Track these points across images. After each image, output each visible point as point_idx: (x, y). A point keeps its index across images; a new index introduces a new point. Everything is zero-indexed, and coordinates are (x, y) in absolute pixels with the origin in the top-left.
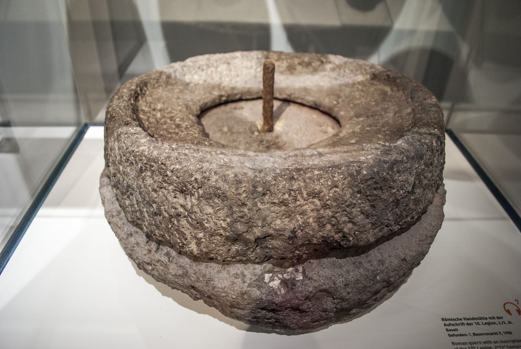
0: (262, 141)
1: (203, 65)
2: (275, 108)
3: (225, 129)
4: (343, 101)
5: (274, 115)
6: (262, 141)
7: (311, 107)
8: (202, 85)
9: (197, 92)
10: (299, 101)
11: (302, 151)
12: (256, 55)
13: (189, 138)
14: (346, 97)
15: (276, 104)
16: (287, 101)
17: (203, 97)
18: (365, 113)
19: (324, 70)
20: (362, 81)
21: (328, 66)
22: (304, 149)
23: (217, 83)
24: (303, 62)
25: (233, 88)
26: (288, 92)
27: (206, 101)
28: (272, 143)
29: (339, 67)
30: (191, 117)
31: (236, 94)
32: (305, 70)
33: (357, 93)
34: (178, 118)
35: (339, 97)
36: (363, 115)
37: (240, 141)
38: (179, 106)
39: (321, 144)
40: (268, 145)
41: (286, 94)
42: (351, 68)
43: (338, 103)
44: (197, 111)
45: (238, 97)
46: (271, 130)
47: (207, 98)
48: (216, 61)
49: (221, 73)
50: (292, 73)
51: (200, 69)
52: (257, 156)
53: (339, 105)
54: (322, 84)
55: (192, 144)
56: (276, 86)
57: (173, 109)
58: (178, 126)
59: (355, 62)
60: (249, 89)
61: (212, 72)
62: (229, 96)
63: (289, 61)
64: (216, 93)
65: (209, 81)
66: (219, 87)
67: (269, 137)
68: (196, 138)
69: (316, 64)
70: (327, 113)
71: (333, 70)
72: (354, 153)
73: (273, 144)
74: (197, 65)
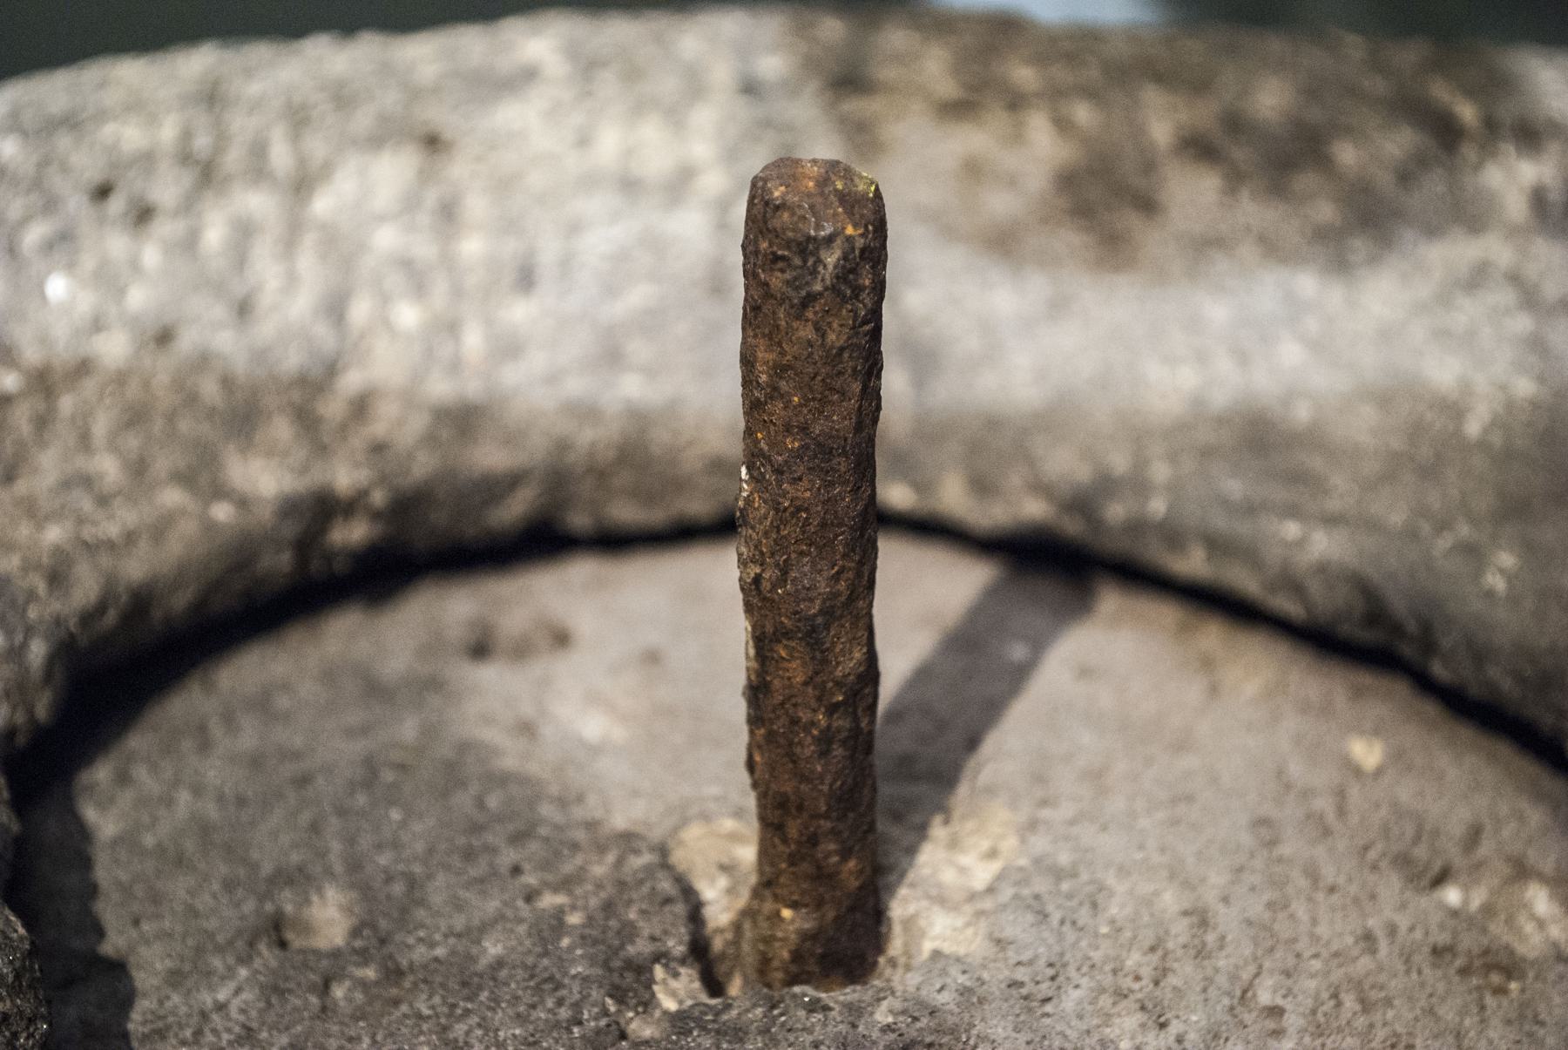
1: (146, 160)
3: (329, 918)
5: (889, 743)
8: (120, 379)
9: (49, 466)
10: (1193, 564)
15: (919, 603)
16: (1060, 563)
19: (1470, 215)
21: (1513, 178)
23: (292, 360)
24: (1235, 124)
25: (462, 420)
26: (1066, 464)
27: (135, 568)
31: (497, 487)
32: (1252, 211)
45: (514, 510)
46: (849, 942)
48: (298, 119)
49: (341, 249)
50: (1113, 250)
51: (116, 204)
54: (1443, 371)
56: (895, 382)
60: (639, 418)
61: (244, 232)
62: (407, 505)
63: (1083, 113)
64: (265, 478)
65: (210, 331)
66: (306, 399)
69: (1374, 150)
74: (87, 164)
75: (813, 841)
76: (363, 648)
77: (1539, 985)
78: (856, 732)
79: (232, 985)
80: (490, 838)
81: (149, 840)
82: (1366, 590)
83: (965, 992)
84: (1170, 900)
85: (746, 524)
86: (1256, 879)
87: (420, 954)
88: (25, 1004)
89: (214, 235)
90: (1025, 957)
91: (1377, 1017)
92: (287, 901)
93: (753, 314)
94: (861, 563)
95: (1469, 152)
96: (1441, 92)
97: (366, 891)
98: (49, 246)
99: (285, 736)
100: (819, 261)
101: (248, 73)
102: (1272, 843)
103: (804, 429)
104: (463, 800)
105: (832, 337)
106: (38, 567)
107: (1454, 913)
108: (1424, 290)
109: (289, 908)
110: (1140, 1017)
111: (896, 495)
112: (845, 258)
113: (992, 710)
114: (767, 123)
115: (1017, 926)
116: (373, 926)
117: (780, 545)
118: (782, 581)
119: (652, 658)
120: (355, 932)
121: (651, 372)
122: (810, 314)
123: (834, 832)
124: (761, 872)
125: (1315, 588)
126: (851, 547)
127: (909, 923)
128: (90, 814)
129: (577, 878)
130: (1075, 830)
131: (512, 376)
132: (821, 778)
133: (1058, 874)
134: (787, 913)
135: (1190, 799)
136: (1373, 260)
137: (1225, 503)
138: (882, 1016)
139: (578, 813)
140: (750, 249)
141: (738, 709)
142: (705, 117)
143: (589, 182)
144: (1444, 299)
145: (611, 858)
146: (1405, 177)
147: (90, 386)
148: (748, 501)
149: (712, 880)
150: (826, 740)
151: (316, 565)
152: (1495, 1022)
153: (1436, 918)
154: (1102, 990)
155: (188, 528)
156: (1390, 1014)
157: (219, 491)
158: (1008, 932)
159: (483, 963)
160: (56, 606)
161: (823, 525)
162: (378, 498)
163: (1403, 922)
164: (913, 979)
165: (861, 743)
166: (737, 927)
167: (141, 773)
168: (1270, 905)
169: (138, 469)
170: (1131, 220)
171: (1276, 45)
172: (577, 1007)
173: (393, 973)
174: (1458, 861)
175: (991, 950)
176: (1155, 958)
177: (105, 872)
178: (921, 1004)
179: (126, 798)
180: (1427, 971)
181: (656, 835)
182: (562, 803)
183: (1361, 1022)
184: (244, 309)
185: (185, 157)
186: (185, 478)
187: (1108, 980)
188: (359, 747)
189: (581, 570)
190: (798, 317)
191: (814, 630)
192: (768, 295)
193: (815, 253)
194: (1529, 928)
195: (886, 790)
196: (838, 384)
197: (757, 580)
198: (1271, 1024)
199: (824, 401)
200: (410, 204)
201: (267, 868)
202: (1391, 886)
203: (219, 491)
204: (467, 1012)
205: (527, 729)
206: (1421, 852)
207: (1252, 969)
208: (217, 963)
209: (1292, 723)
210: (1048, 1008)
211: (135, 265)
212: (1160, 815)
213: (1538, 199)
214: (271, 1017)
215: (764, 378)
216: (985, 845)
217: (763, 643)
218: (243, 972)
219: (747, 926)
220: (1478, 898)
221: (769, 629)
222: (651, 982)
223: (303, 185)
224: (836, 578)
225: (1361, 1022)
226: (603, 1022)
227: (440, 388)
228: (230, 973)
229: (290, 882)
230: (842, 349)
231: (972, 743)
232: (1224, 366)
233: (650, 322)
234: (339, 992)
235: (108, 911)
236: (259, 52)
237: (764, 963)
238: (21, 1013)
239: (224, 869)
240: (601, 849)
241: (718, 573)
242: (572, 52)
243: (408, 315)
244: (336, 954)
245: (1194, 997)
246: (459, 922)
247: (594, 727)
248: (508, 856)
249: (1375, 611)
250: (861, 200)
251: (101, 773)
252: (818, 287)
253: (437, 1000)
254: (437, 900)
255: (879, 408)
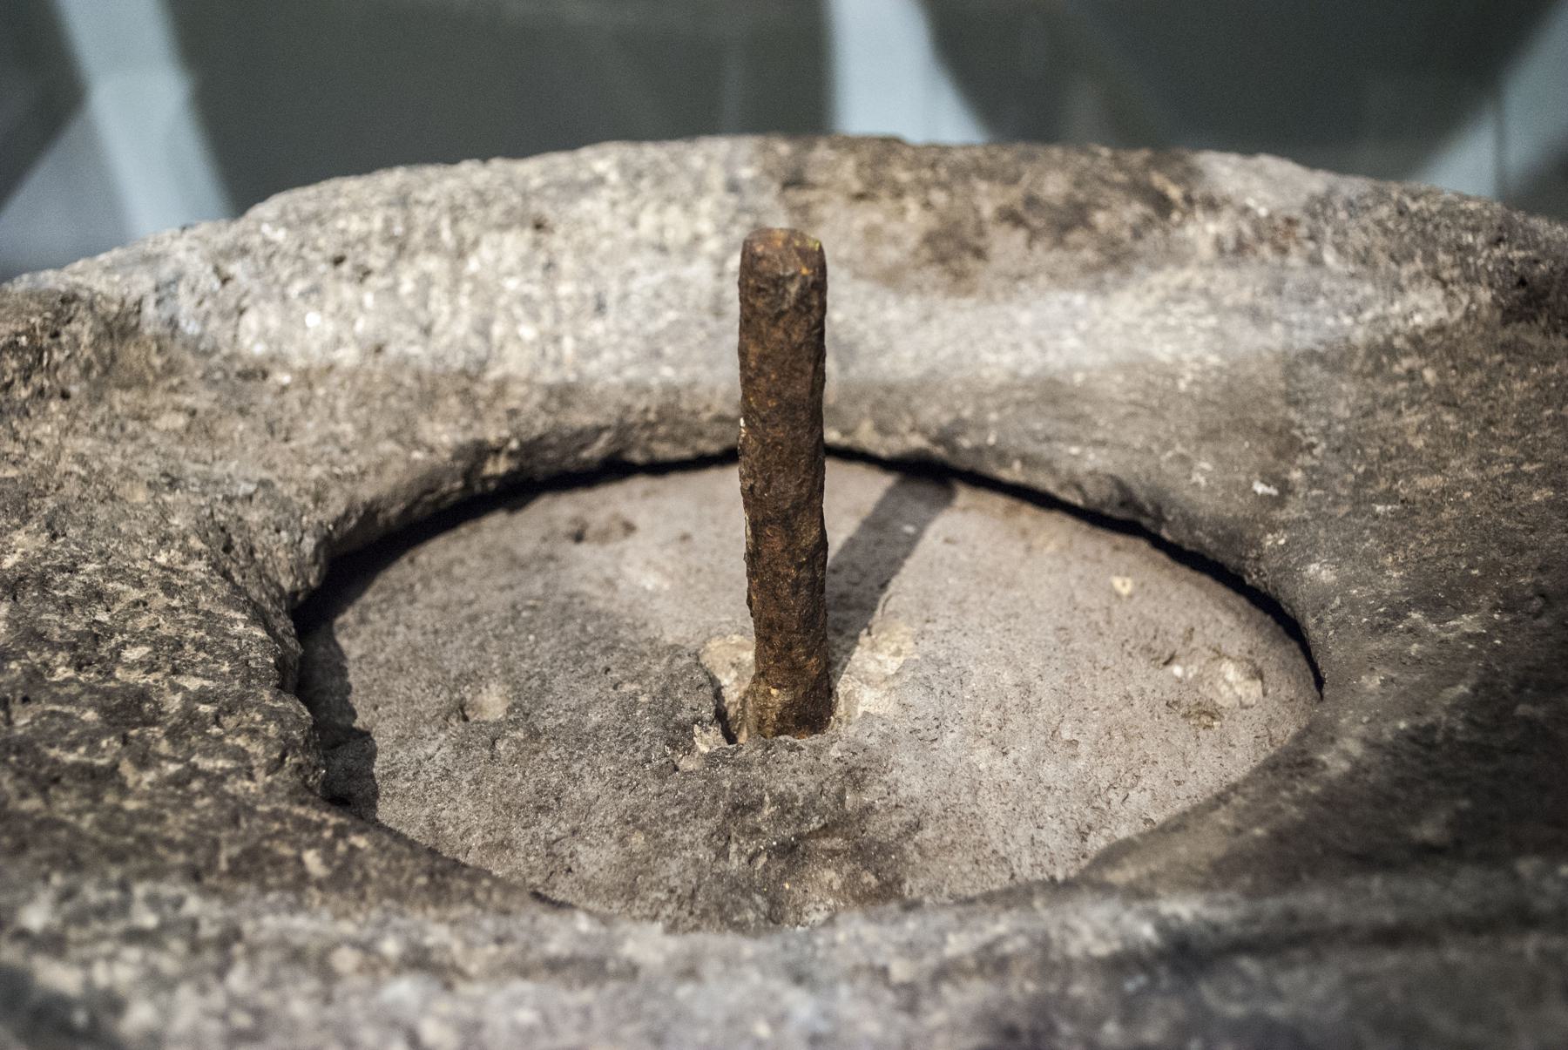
0: (743, 807)
1: (364, 240)
2: (838, 536)
3: (493, 702)
4: (1317, 477)
5: (835, 584)
6: (743, 807)
7: (1093, 517)
8: (353, 375)
9: (310, 431)
10: (1013, 473)
11: (1045, 915)
12: (723, 162)
13: (176, 825)
14: (1343, 447)
15: (850, 499)
16: (933, 474)
17: (360, 459)
18: (1492, 568)
19: (1177, 256)
20: (1440, 329)
21: (1203, 232)
22: (1060, 889)
23: (458, 362)
24: (1031, 201)
25: (563, 395)
26: (935, 414)
27: (366, 492)
28: (815, 823)
29: (1276, 233)
30: (239, 624)
31: (586, 436)
32: (1043, 255)
33: (1412, 418)
34: (138, 639)
35: (1289, 446)
36: (1476, 585)
37: (587, 809)
38: (164, 541)
39: (1183, 849)
40: (788, 833)
41: (924, 431)
42: (1358, 239)
43: (1286, 488)
44: (297, 568)
45: (597, 450)
46: (812, 709)
47: (384, 471)
48: (456, 212)
49: (485, 291)
50: (960, 282)
51: (346, 268)
52: (690, 973)
53: (1292, 511)
54: (1164, 351)
55: (195, 875)
57: (110, 573)
58: (128, 711)
59: (1382, 197)
60: (671, 389)
61: (426, 281)
62: (530, 449)
63: (939, 197)
64: (443, 435)
65: (405, 344)
66: (468, 384)
67: (795, 769)
68: (238, 811)
69: (1118, 215)
70: (1212, 560)
71: (1236, 251)
72: (1453, 955)
73: (826, 831)
74: (328, 244)
75: (790, 648)
76: (507, 537)
77: (1231, 723)
78: (814, 580)
79: (436, 744)
80: (589, 650)
81: (381, 658)
82: (1120, 485)
83: (884, 736)
84: (1007, 678)
85: (744, 453)
86: (1058, 664)
87: (550, 722)
88: (312, 758)
89: (407, 286)
90: (920, 715)
91: (1134, 745)
92: (467, 692)
93: (746, 324)
94: (816, 476)
95: (1176, 216)
96: (1158, 180)
97: (515, 685)
98: (304, 295)
99: (458, 591)
100: (786, 291)
101: (427, 184)
102: (1068, 642)
103: (779, 394)
104: (572, 628)
105: (795, 337)
106: (307, 492)
107: (1180, 681)
108: (1150, 301)
109: (469, 697)
110: (991, 749)
111: (832, 436)
112: (802, 288)
113: (895, 564)
114: (742, 210)
115: (915, 696)
116: (521, 707)
117: (765, 467)
118: (767, 488)
119: (685, 538)
120: (510, 710)
121: (677, 366)
122: (781, 324)
123: (802, 641)
124: (758, 667)
125: (1089, 485)
126: (809, 466)
127: (848, 696)
128: (344, 642)
129: (645, 673)
130: (949, 636)
131: (592, 367)
132: (794, 609)
133: (939, 664)
134: (774, 692)
135: (1017, 616)
136: (1119, 286)
137: (1033, 435)
138: (834, 752)
139: (643, 634)
140: (743, 285)
141: (741, 568)
142: (705, 205)
143: (635, 246)
144: (1163, 306)
145: (665, 661)
146: (1137, 234)
147: (335, 379)
148: (745, 440)
149: (728, 673)
150: (796, 585)
151: (478, 488)
152: (1205, 746)
153: (1168, 684)
154: (968, 733)
155: (399, 465)
156: (1142, 742)
157: (417, 444)
158: (910, 700)
159: (588, 728)
160: (320, 515)
161: (792, 453)
162: (514, 445)
163: (1149, 687)
164: (853, 730)
165: (817, 587)
166: (744, 701)
167: (373, 616)
168: (1068, 679)
169: (366, 430)
170: (970, 263)
171: (1056, 152)
172: (648, 751)
173: (534, 735)
174: (1180, 650)
175: (899, 711)
176: (999, 713)
177: (355, 677)
178: (857, 744)
179: (365, 632)
180: (1164, 716)
181: (692, 646)
182: (634, 628)
183: (1125, 748)
184: (427, 331)
185: (388, 239)
186: (393, 435)
187: (971, 727)
188: (508, 596)
189: (639, 484)
190: (774, 325)
191: (787, 518)
192: (755, 312)
193: (783, 286)
194: (1224, 688)
195: (832, 615)
196: (799, 366)
197: (752, 488)
198: (1070, 751)
199: (791, 377)
200: (526, 262)
201: (454, 673)
202: (1140, 666)
203: (417, 444)
204: (580, 757)
205: (610, 583)
206: (1157, 645)
207: (1058, 718)
208: (426, 731)
209: (1077, 569)
210: (935, 745)
211: (361, 304)
212: (998, 626)
213: (1219, 243)
214: (460, 763)
215: (753, 364)
216: (893, 647)
217: (756, 527)
218: (442, 736)
219: (749, 700)
220: (1193, 670)
221: (760, 518)
222: (693, 735)
223: (460, 254)
224: (800, 486)
225: (1125, 748)
226: (664, 761)
227: (549, 376)
228: (434, 737)
229: (469, 681)
230: (801, 345)
231: (883, 586)
232: (1030, 350)
233: (677, 332)
234: (501, 746)
235: (357, 701)
236: (431, 171)
237: (761, 722)
238: (309, 763)
239: (427, 674)
240: (659, 656)
241: (728, 483)
242: (623, 166)
243: (528, 332)
244: (498, 724)
245: (1023, 736)
246: (573, 703)
247: (650, 581)
248: (602, 662)
249: (1127, 499)
250: (812, 252)
251: (349, 616)
252: (785, 307)
253: (561, 750)
254: (559, 689)
255: (824, 380)
